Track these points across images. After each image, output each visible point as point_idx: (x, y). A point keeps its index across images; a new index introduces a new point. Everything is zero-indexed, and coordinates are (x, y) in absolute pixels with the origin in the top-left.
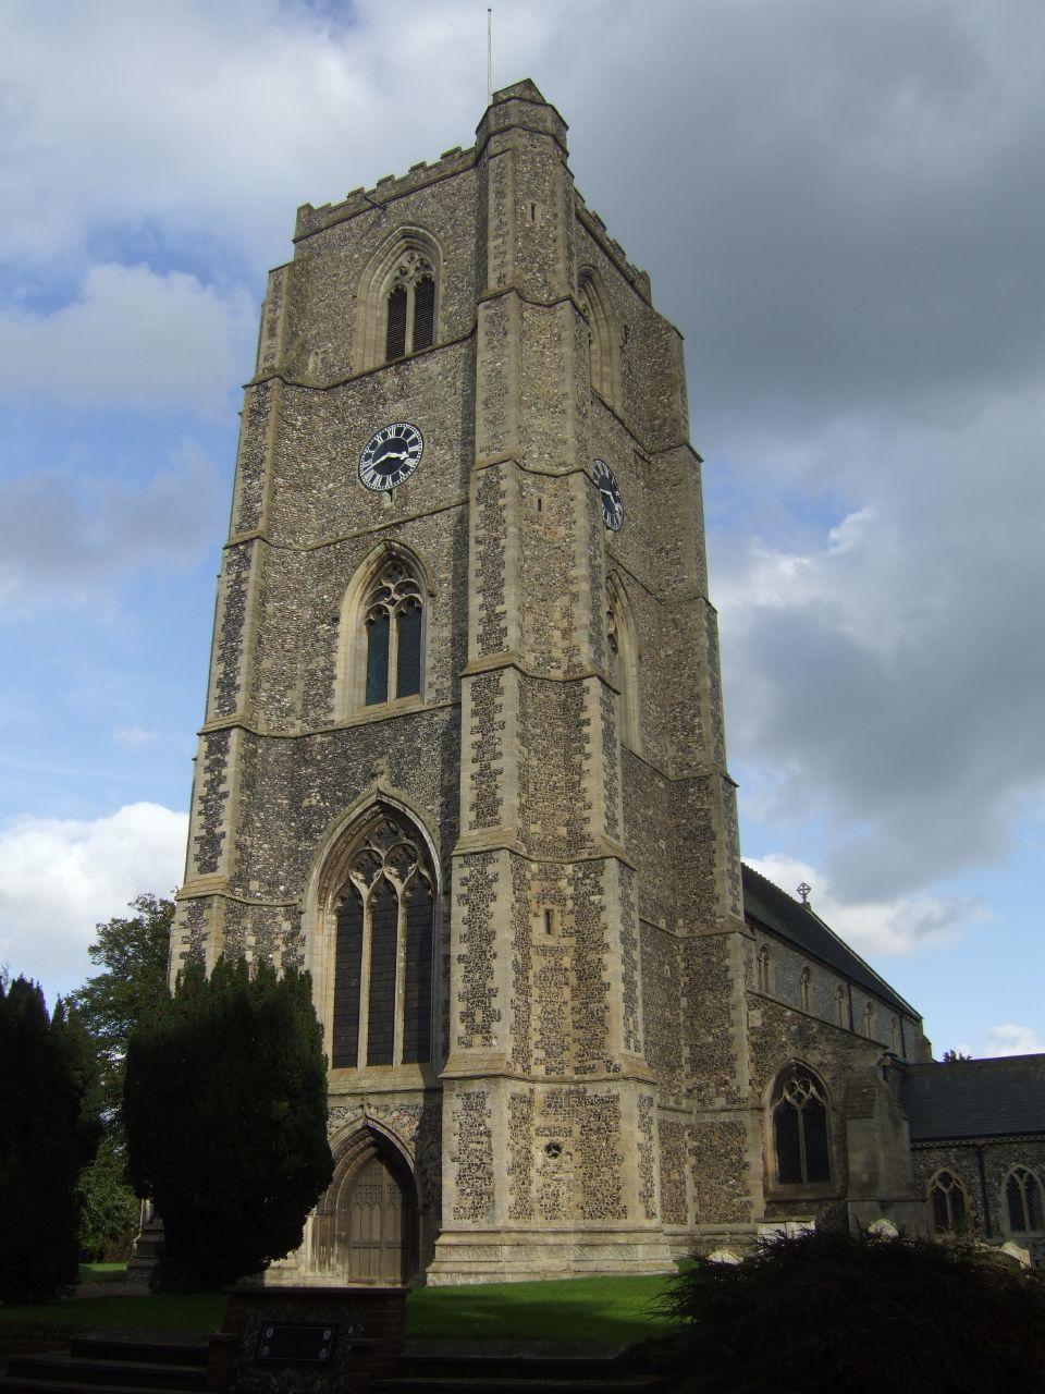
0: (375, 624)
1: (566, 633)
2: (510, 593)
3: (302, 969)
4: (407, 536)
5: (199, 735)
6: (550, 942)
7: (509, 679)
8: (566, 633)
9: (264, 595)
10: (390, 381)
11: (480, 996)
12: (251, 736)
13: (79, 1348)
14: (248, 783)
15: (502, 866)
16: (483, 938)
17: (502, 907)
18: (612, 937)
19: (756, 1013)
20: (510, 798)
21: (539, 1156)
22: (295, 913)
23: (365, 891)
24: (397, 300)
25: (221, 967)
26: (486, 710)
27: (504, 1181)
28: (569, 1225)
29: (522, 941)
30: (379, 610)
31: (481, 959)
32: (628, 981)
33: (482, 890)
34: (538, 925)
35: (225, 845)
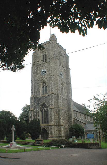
0: (43, 87)
1: (57, 90)
2: (53, 87)
3: (77, 31)
4: (45, 80)
5: (28, 55)
6: (56, 115)
7: (53, 94)
8: (57, 90)
9: (34, 85)
10: (43, 65)
11: (51, 119)
12: (34, 97)
13: (28, 143)
14: (34, 101)
15: (53, 110)
16: (51, 115)
17: (53, 112)
18: (61, 115)
19: (74, 119)
20: (53, 104)
21: (56, 131)
22: (38, 111)
23: (43, 110)
24: (43, 56)
25: (34, 120)
26: (51, 97)
27: (53, 133)
28: (58, 136)
29: (54, 115)
30: (43, 86)
31: (51, 116)
32: (62, 118)
33: (51, 112)
34: (56, 114)
35: (33, 106)
